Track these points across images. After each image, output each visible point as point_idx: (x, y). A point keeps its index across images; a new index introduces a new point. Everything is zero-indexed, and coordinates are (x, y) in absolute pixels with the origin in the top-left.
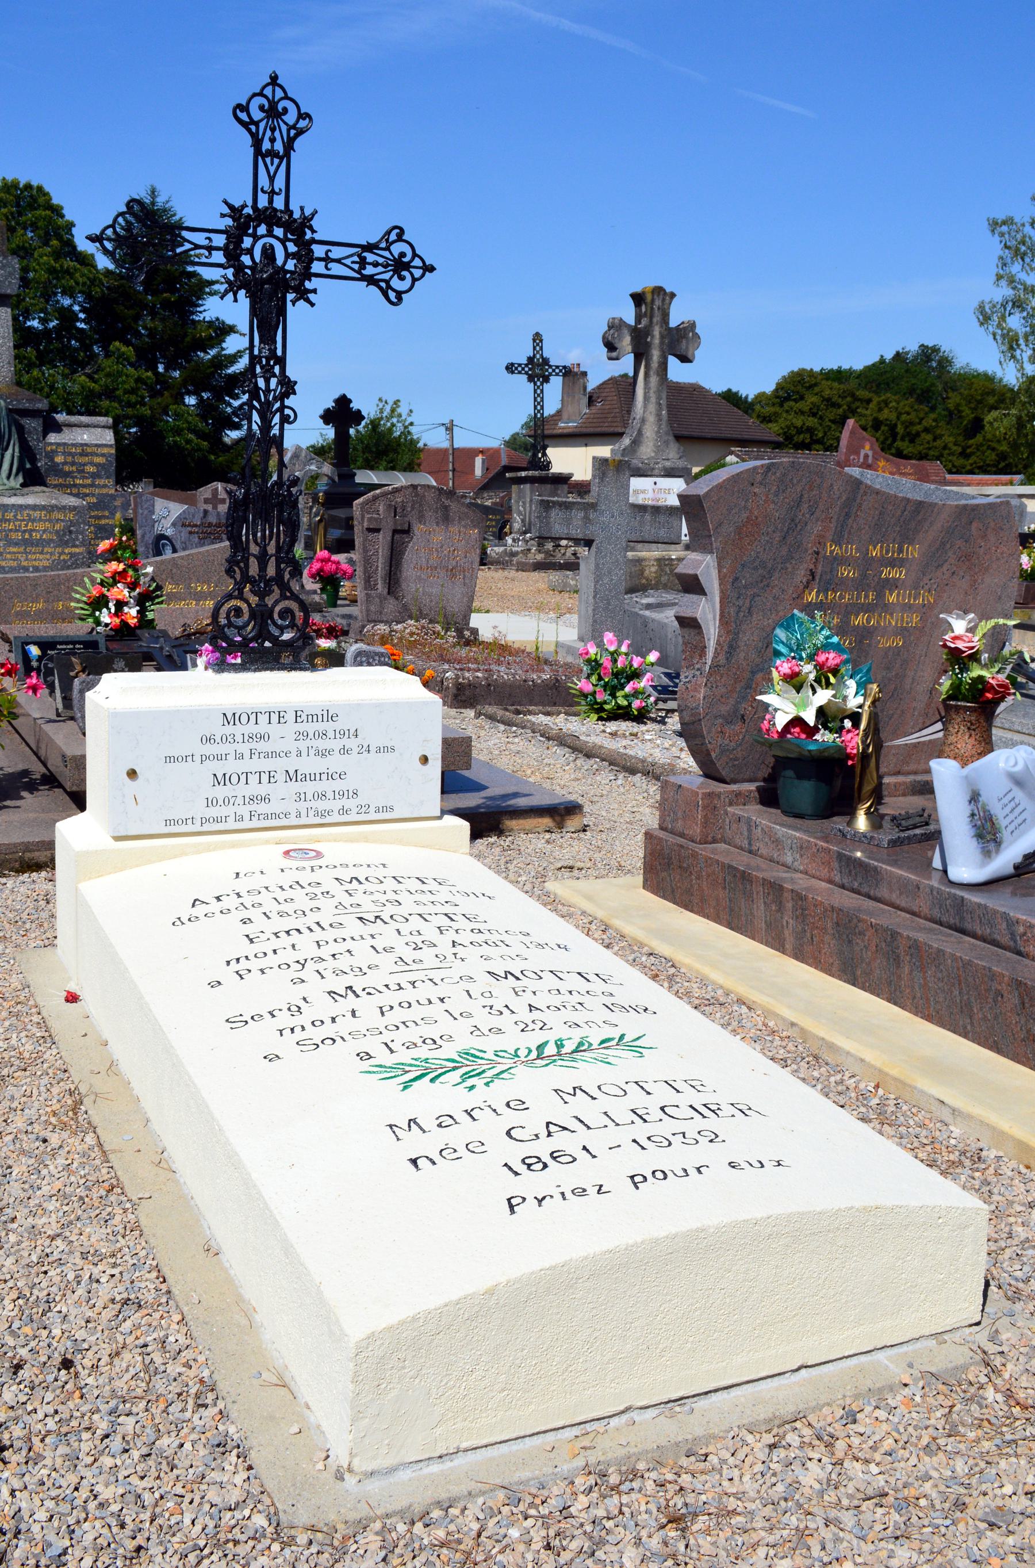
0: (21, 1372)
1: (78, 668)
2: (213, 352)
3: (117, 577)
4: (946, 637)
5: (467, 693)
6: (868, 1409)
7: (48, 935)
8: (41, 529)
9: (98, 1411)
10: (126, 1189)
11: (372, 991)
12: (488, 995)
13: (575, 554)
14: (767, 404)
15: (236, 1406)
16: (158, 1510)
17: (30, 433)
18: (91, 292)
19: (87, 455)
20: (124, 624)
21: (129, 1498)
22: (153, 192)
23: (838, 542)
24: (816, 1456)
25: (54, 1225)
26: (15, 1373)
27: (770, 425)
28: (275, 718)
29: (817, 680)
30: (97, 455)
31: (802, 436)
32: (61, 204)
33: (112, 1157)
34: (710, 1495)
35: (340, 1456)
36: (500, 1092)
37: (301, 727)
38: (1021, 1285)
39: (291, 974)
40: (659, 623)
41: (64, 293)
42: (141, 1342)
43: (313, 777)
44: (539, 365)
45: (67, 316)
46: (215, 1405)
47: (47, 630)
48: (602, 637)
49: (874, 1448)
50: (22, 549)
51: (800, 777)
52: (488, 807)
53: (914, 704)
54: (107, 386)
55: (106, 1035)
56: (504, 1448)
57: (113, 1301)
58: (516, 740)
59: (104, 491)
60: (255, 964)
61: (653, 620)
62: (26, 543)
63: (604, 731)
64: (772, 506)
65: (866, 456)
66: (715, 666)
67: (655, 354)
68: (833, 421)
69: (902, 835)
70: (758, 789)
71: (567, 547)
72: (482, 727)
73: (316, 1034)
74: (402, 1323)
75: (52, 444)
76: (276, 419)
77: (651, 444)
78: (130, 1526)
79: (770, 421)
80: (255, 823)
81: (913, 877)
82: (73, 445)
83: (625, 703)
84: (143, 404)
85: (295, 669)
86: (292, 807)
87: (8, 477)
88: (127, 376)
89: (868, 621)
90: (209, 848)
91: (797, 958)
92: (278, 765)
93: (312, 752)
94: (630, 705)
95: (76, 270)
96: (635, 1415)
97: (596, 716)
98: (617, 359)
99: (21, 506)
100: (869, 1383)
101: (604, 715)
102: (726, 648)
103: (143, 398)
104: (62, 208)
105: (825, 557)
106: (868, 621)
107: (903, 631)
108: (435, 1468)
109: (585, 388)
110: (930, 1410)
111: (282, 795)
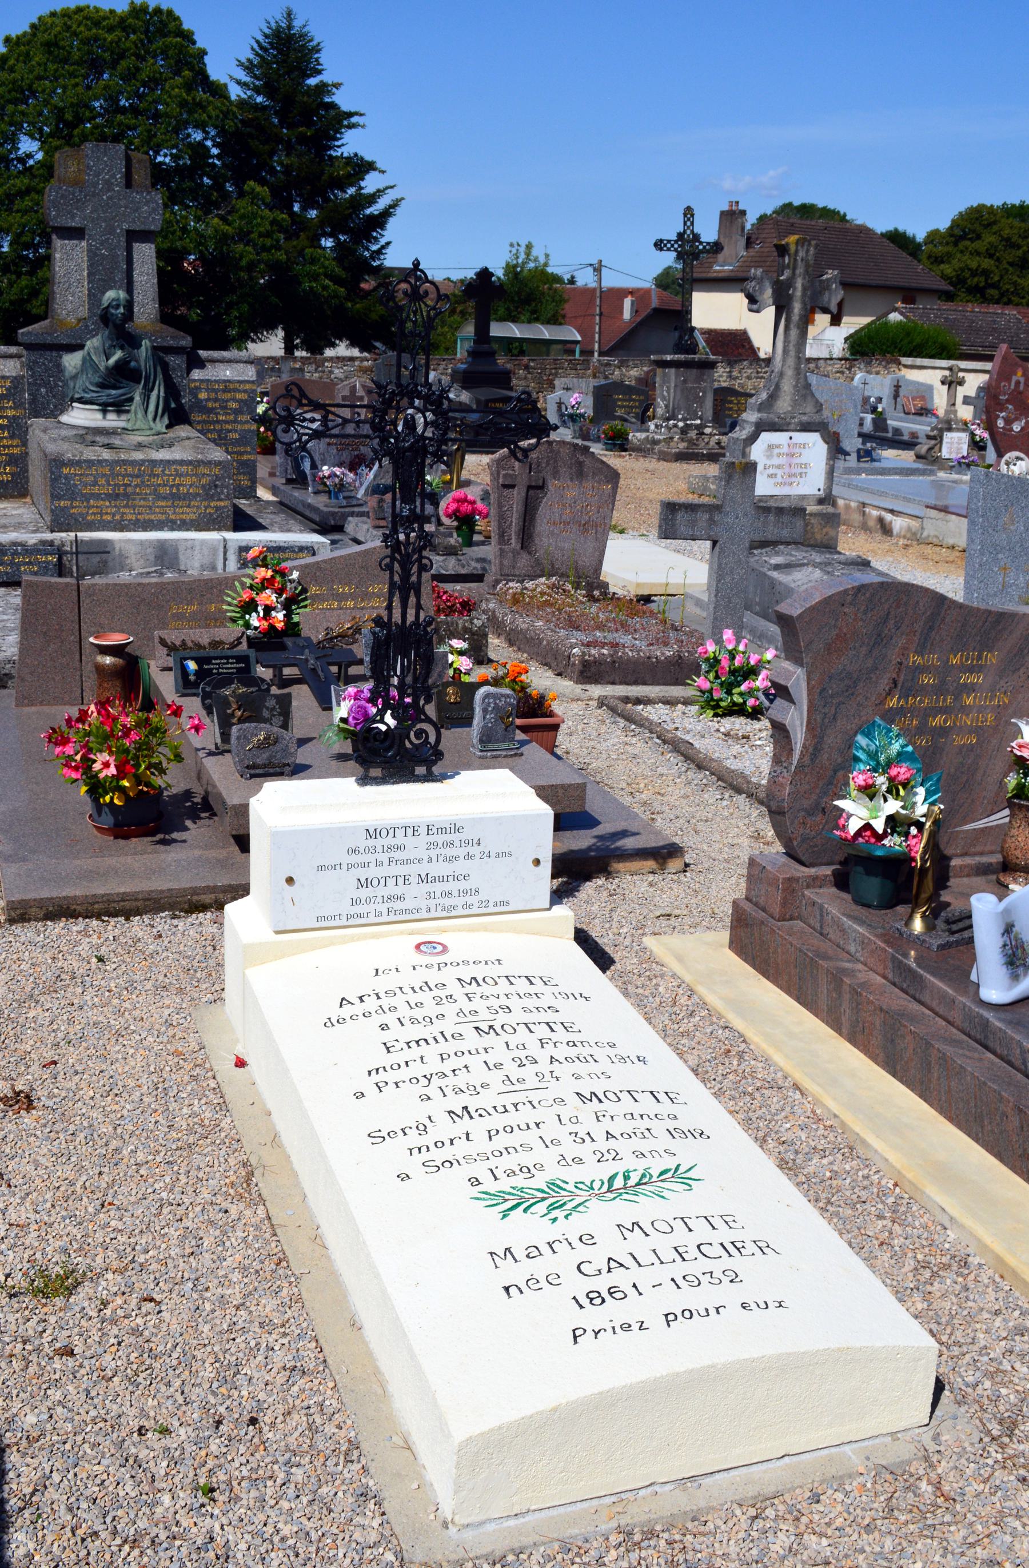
0: (221, 1427)
1: (234, 706)
2: (351, 191)
3: (266, 584)
4: (1014, 744)
5: (593, 669)
6: (830, 1492)
7: (217, 987)
8: (187, 483)
9: (276, 1462)
10: (291, 1264)
11: (484, 1113)
12: (574, 1120)
13: (718, 443)
14: (941, 243)
15: (374, 1464)
16: (321, 1545)
17: (174, 369)
18: (223, 126)
19: (229, 391)
20: (272, 627)
21: (301, 1534)
22: (289, 14)
23: (920, 653)
24: (785, 1528)
25: (238, 1296)
26: (217, 1428)
27: (942, 266)
28: (410, 831)
29: (889, 791)
30: (239, 391)
31: (976, 279)
32: (192, 28)
33: (278, 1231)
34: (704, 1554)
35: (447, 1510)
36: (574, 1226)
37: (432, 839)
38: (970, 1390)
39: (419, 1089)
40: (786, 587)
41: (196, 127)
42: (305, 1404)
43: (441, 879)
44: (689, 241)
45: (199, 151)
46: (359, 1462)
47: (203, 636)
48: (721, 633)
49: (829, 1524)
50: (170, 503)
51: (868, 873)
52: (598, 849)
53: (984, 793)
54: (241, 229)
55: (270, 1105)
56: (562, 1510)
57: (284, 1368)
58: (634, 740)
59: (246, 427)
60: (391, 1076)
61: (780, 583)
62: (175, 497)
63: (718, 730)
64: (861, 623)
65: (1018, 383)
66: (800, 766)
67: (797, 307)
68: (1011, 264)
69: (952, 939)
70: (835, 873)
71: (711, 435)
72: (603, 722)
73: (438, 1155)
74: (492, 1430)
75: (195, 381)
76: (415, 569)
77: (788, 398)
78: (302, 1556)
79: (942, 262)
80: (392, 918)
81: (950, 991)
82: (216, 381)
83: (741, 701)
84: (278, 248)
85: (428, 781)
86: (423, 904)
87: (154, 419)
88: (262, 218)
89: (945, 721)
90: (353, 939)
91: (850, 1041)
92: (413, 870)
93: (441, 859)
94: (745, 702)
95: (209, 103)
96: (657, 1488)
97: (711, 713)
98: (758, 311)
99: (168, 461)
100: (833, 1471)
101: (719, 711)
102: (811, 750)
103: (278, 241)
104: (193, 33)
105: (907, 667)
106: (945, 721)
107: (976, 731)
108: (512, 1523)
109: (743, 228)
110: (876, 1495)
111: (415, 895)
